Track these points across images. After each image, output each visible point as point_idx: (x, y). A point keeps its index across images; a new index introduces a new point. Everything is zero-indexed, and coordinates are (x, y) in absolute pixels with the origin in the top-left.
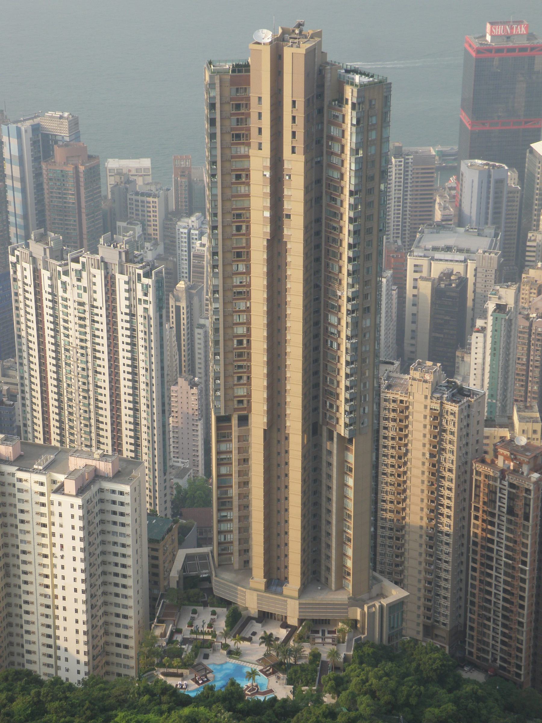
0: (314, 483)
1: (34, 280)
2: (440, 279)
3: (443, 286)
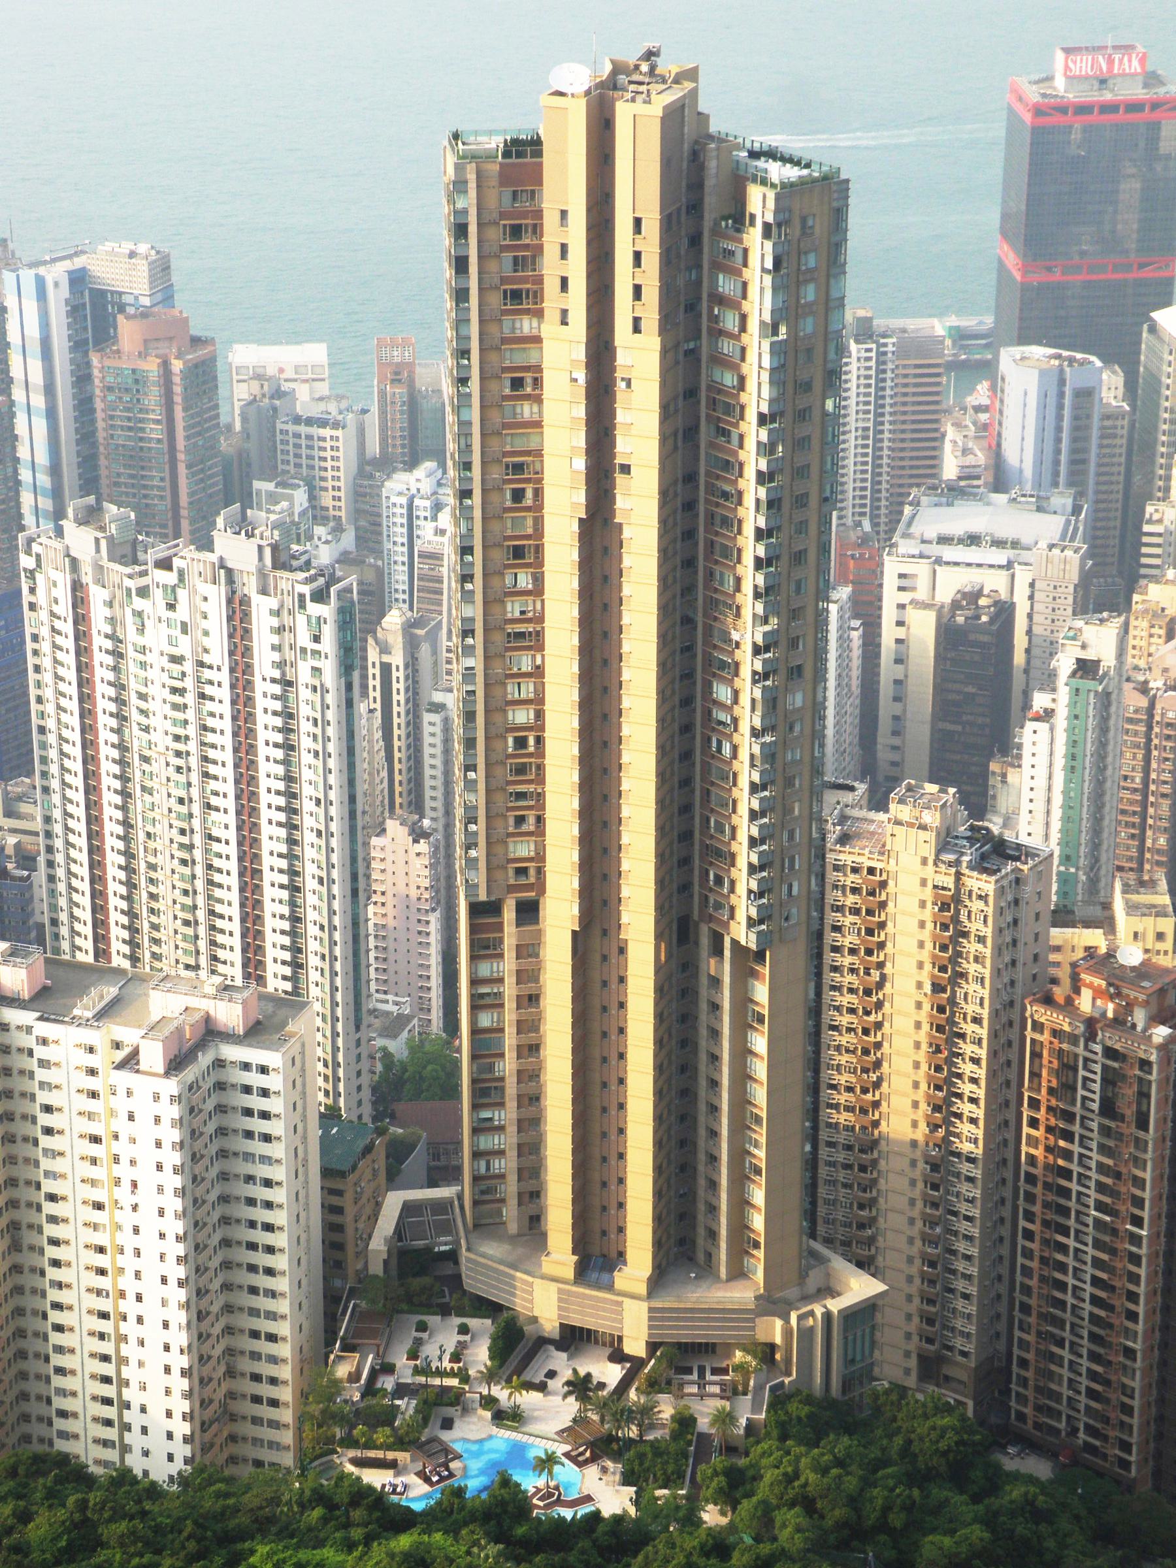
1: (74, 606)
2: (955, 605)
3: (960, 620)
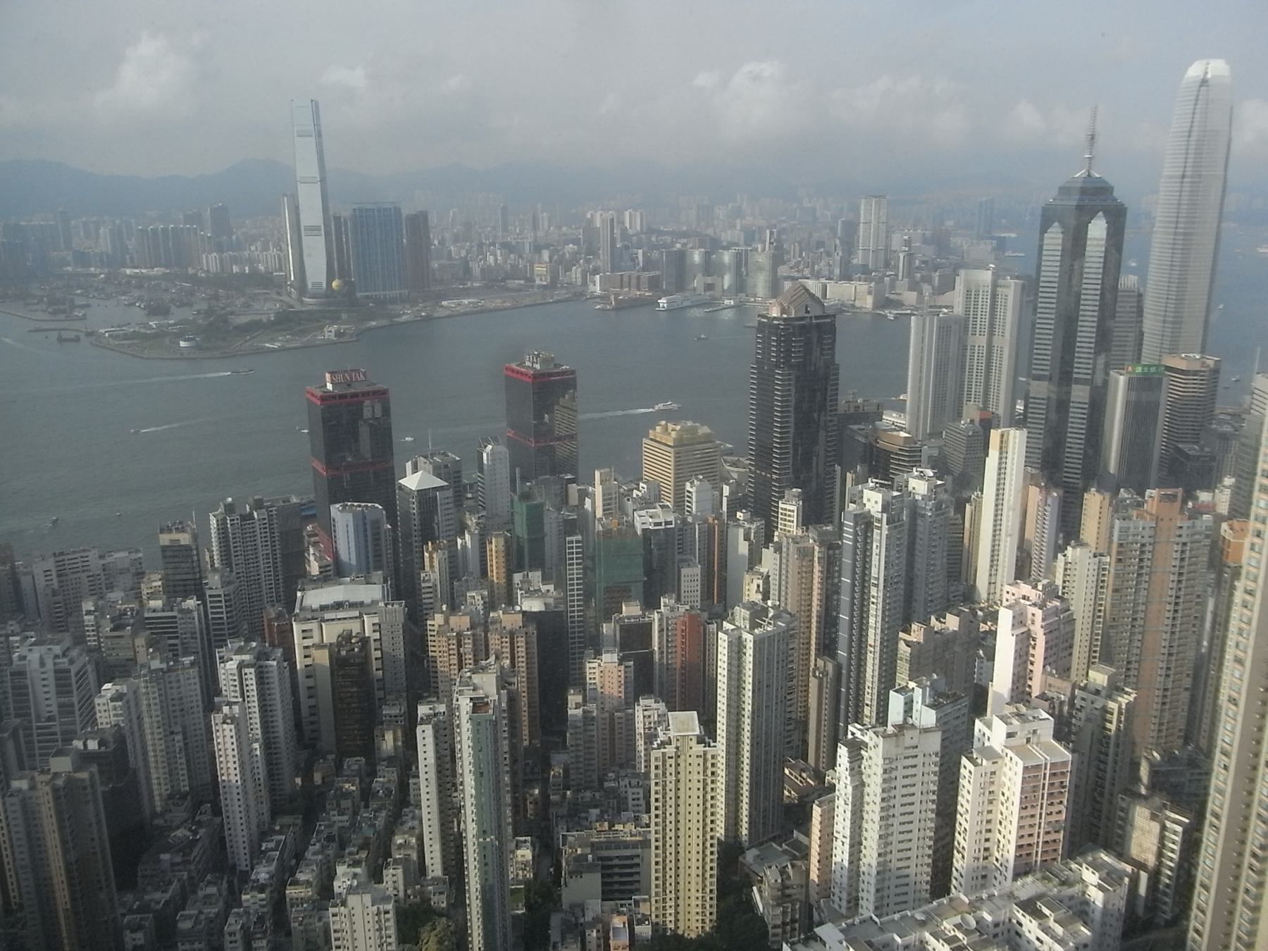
2: (339, 645)
3: (343, 653)
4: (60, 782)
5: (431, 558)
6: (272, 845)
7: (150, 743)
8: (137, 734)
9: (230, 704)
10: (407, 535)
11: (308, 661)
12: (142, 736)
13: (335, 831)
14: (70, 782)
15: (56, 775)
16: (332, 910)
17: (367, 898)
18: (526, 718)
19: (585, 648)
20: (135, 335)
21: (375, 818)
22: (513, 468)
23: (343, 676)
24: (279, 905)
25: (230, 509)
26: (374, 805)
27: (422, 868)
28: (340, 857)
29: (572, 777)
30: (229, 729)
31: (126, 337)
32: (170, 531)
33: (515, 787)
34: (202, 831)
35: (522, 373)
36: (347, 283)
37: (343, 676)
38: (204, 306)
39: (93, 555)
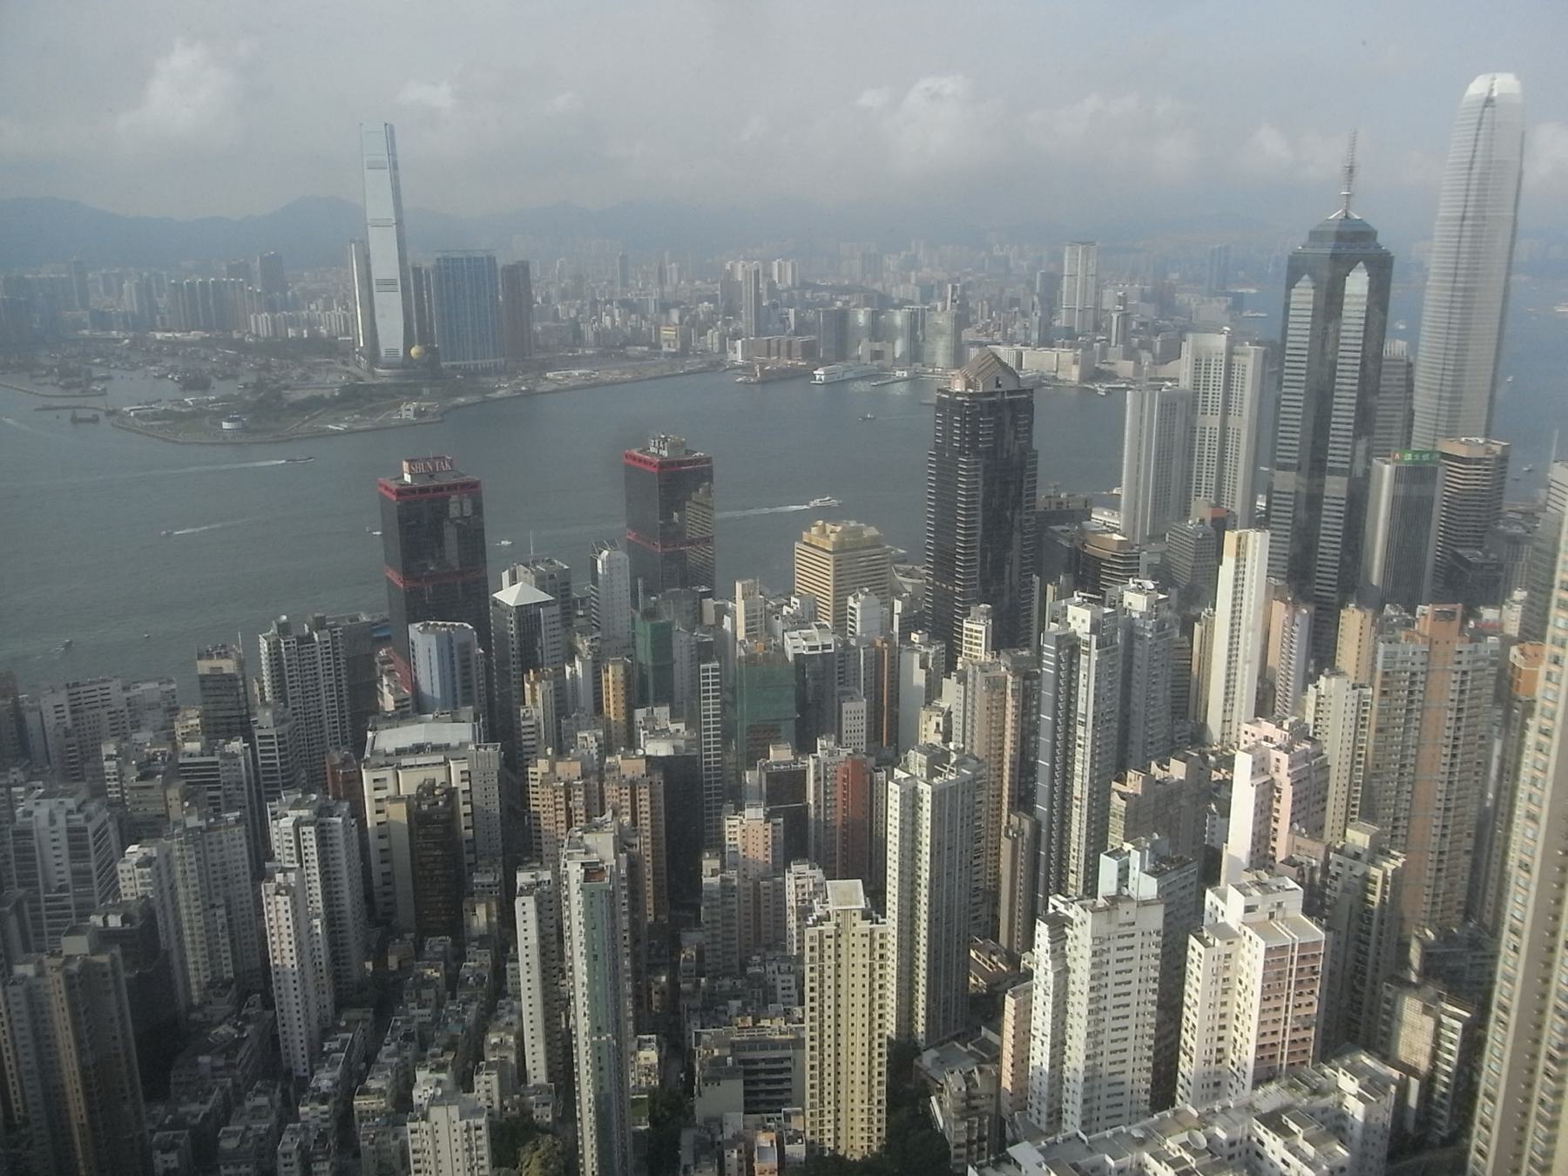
0: (177, 709)
2: (419, 797)
3: (425, 807)
4: (74, 967)
5: (533, 690)
6: (336, 1045)
7: (185, 918)
8: (169, 908)
9: (284, 871)
10: (504, 662)
11: (381, 818)
12: (176, 910)
13: (414, 1027)
14: (87, 966)
15: (70, 958)
16: (410, 1126)
17: (454, 1111)
18: (650, 888)
19: (723, 801)
20: (168, 414)
21: (464, 1011)
22: (634, 578)
23: (424, 836)
24: (345, 1119)
25: (284, 629)
26: (462, 995)
27: (522, 1073)
28: (420, 1060)
29: (708, 961)
30: (283, 902)
31: (156, 416)
32: (210, 656)
33: (637, 973)
34: (250, 1028)
35: (645, 462)
36: (429, 350)
37: (424, 836)
38: (253, 379)
39: (115, 686)
